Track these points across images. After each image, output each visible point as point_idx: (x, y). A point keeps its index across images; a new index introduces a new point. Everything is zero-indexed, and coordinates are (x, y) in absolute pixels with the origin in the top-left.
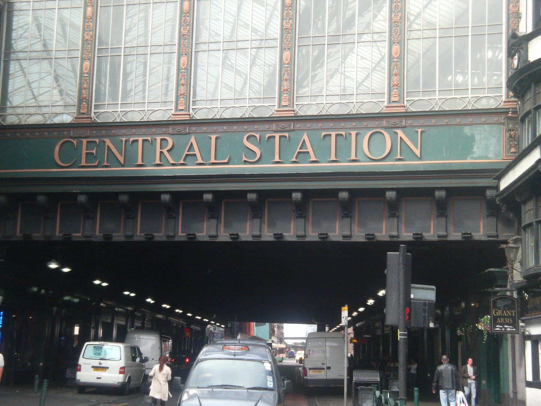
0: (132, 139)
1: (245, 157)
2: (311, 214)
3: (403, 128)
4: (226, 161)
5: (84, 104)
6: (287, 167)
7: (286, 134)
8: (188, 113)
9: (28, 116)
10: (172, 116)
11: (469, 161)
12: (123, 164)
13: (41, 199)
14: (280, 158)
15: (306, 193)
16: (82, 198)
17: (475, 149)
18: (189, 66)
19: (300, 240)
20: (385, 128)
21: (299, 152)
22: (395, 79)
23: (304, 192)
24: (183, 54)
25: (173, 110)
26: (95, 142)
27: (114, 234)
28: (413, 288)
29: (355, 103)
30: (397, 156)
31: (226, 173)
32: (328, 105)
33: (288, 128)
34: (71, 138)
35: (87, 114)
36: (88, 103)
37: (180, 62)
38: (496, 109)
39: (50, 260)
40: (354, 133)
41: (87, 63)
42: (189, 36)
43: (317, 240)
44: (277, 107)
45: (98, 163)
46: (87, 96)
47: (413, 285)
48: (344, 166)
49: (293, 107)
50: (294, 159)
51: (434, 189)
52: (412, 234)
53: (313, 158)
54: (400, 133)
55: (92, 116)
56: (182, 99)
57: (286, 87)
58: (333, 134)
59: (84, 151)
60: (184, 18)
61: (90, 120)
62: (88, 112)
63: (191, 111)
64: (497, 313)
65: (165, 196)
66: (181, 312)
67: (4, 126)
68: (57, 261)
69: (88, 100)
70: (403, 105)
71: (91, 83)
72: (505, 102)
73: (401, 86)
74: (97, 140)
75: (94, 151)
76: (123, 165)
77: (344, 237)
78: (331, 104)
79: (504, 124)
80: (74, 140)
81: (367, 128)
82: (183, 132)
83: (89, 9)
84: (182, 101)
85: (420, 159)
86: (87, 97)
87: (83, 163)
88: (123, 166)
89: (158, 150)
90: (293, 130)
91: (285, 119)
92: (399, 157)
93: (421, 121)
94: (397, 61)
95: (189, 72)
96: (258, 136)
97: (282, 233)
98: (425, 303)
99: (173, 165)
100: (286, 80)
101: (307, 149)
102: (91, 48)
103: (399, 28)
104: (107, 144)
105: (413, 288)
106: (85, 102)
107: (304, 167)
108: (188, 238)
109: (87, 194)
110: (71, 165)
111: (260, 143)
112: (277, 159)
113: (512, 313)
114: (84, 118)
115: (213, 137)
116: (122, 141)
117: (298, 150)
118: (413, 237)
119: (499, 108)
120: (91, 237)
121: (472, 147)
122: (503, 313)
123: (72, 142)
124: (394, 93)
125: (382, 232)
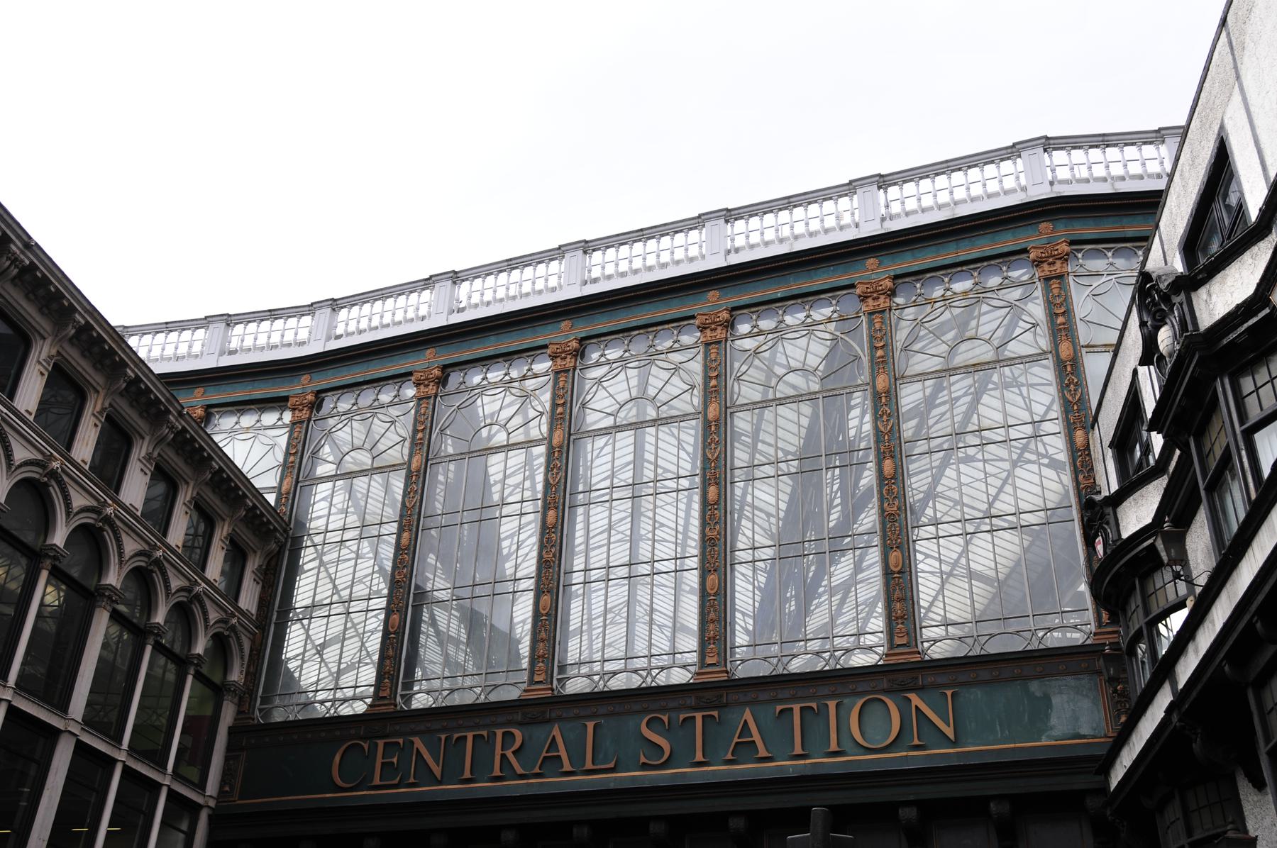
0: (456, 736)
4: (612, 765)
6: (719, 771)
7: (715, 713)
8: (550, 686)
9: (791, 657)
10: (696, 677)
11: (1045, 742)
12: (439, 779)
14: (704, 756)
15: (923, 806)
17: (1054, 721)
18: (554, 609)
20: (886, 692)
21: (545, 757)
22: (711, 628)
23: (749, 815)
30: (409, 778)
34: (361, 738)
35: (390, 699)
36: (392, 681)
37: (705, 585)
42: (405, 582)
45: (400, 779)
48: (821, 762)
50: (729, 757)
54: (915, 699)
55: (554, 687)
56: (541, 664)
59: (379, 761)
60: (709, 513)
62: (390, 696)
63: (555, 682)
65: (907, 810)
69: (393, 675)
70: (916, 649)
72: (1095, 634)
73: (720, 639)
74: (401, 741)
75: (395, 760)
76: (954, 743)
79: (1101, 672)
82: (911, 684)
83: (551, 513)
84: (901, 629)
85: (954, 743)
87: (377, 781)
88: (440, 783)
89: (498, 751)
92: (916, 742)
94: (899, 577)
95: (553, 620)
96: (665, 719)
99: (522, 777)
100: (712, 621)
102: (404, 593)
103: (897, 525)
104: (415, 746)
106: (388, 678)
107: (747, 769)
111: (667, 731)
112: (699, 757)
115: (590, 725)
116: (440, 739)
119: (1087, 645)
121: (1048, 717)
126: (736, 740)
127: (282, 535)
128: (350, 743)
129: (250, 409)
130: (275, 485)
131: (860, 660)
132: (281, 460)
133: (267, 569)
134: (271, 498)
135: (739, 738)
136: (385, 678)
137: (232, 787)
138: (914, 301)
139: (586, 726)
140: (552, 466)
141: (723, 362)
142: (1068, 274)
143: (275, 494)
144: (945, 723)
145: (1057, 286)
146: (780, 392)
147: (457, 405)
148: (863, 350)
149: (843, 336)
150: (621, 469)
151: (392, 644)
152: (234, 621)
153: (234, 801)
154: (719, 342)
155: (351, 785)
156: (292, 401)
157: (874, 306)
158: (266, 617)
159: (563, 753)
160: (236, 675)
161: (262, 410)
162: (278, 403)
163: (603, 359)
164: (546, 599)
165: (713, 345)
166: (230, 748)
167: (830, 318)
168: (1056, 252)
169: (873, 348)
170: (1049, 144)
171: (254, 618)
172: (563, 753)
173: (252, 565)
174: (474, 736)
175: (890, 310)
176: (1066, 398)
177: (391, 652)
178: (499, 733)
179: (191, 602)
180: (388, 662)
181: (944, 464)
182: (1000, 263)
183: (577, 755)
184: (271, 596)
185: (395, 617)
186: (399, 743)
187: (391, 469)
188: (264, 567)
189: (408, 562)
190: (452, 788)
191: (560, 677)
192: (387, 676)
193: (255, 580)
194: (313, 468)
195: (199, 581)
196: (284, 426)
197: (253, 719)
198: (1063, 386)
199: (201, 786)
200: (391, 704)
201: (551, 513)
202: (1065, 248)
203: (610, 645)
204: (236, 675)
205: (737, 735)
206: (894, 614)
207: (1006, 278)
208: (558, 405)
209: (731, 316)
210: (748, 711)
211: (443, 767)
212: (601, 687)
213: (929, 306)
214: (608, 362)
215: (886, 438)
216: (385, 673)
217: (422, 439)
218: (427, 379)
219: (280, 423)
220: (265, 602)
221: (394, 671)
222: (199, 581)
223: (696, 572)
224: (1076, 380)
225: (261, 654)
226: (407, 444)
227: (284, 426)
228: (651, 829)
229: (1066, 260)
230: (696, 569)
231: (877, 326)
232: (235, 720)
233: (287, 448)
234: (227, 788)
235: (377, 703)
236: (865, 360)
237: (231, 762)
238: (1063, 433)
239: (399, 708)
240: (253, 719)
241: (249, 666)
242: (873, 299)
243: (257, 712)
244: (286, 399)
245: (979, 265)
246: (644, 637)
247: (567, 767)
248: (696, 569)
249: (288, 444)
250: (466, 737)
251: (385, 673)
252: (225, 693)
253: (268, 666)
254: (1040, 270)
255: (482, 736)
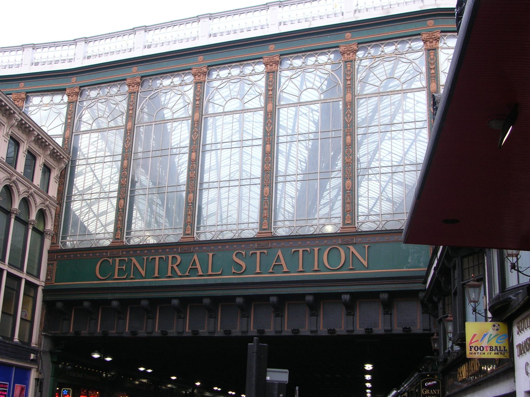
0: (151, 257)
1: (234, 269)
2: (321, 313)
3: (353, 244)
4: (220, 273)
5: (188, 227)
6: (266, 276)
7: (265, 251)
13: (115, 303)
14: (260, 270)
16: (115, 303)
19: (244, 335)
20: (340, 245)
21: (191, 268)
24: (347, 179)
25: (341, 224)
26: (307, 250)
27: (139, 331)
28: (269, 371)
29: (318, 225)
30: (350, 266)
31: (219, 282)
32: (298, 228)
33: (351, 242)
34: (109, 257)
36: (191, 226)
38: (375, 231)
39: (94, 351)
40: (316, 249)
41: (191, 195)
43: (291, 335)
44: (342, 225)
45: (126, 277)
46: (191, 220)
47: (268, 369)
48: (309, 275)
49: (355, 224)
50: (271, 271)
51: (341, 294)
52: (364, 329)
53: (285, 269)
55: (195, 236)
57: (348, 209)
58: (301, 250)
60: (266, 158)
61: (193, 239)
62: (191, 233)
64: (426, 392)
65: (345, 296)
66: (234, 393)
67: (63, 249)
68: (99, 352)
70: (354, 226)
71: (271, 205)
74: (126, 259)
75: (124, 267)
77: (312, 332)
78: (323, 226)
80: (110, 259)
81: (327, 245)
84: (348, 216)
85: (367, 268)
86: (267, 216)
87: (116, 276)
88: (144, 278)
90: (271, 248)
91: (351, 234)
92: (351, 267)
93: (368, 239)
94: (350, 193)
96: (244, 253)
97: (264, 330)
98: (281, 385)
99: (180, 276)
101: (196, 266)
105: (269, 371)
107: (279, 276)
108: (162, 334)
109: (119, 300)
110: (105, 279)
113: (437, 392)
114: (118, 242)
115: (211, 255)
116: (144, 259)
117: (274, 263)
118: (365, 332)
119: (213, 240)
120: (122, 333)
122: (430, 392)
123: (108, 260)
124: (347, 217)
125: (341, 327)
126: (190, 267)
127: (67, 160)
128: (331, 247)
129: (47, 94)
130: (62, 134)
131: (329, 229)
132: (64, 121)
133: (61, 176)
134: (59, 141)
135: (191, 266)
136: (118, 230)
137: (51, 277)
138: (367, 57)
139: (209, 255)
140: (347, 113)
141: (74, 111)
142: (438, 48)
143: (62, 138)
144: (364, 259)
145: (433, 54)
146: (110, 125)
147: (148, 97)
148: (341, 81)
149: (332, 72)
150: (185, 139)
151: (190, 208)
152: (47, 203)
153: (53, 283)
154: (202, 82)
155: (105, 278)
156: (68, 91)
157: (430, 46)
158: (61, 199)
159: (198, 266)
160: (50, 226)
161: (53, 95)
162: (61, 91)
163: (218, 77)
164: (267, 189)
165: (349, 63)
166: (49, 259)
167: (326, 62)
168: (434, 37)
169: (346, 80)
170: (212, 17)
171: (56, 199)
172: (198, 266)
173: (55, 174)
174: (159, 258)
175: (355, 61)
176: (266, 129)
177: (120, 218)
178: (170, 257)
179: (29, 197)
180: (119, 222)
181: (382, 140)
182: (408, 40)
183: (205, 269)
184: (63, 189)
185: (122, 201)
186: (125, 260)
187: (117, 128)
188: (59, 175)
189: (196, 168)
190: (149, 281)
191: (197, 232)
192: (119, 229)
193: (55, 182)
194: (79, 127)
195: (32, 187)
196: (64, 103)
197: (59, 247)
198: (266, 124)
199: (38, 277)
200: (121, 242)
201: (126, 162)
202: (355, 47)
203: (230, 216)
204: (50, 226)
205: (275, 261)
206: (346, 209)
207: (410, 48)
208: (197, 100)
209: (280, 59)
210: (280, 251)
211: (368, 260)
212: (318, 231)
213: (374, 59)
214: (220, 79)
215: (349, 125)
216: (118, 228)
217: (131, 114)
218: (133, 83)
219: (62, 102)
220: (60, 192)
221: (122, 226)
222: (32, 187)
223: (259, 186)
224: (351, 112)
225: (60, 217)
226: (190, 107)
227: (64, 103)
228: (172, 302)
229: (438, 41)
230: (260, 184)
231: (349, 68)
232: (51, 247)
233: (67, 115)
234: (49, 277)
235: (115, 241)
236: (341, 85)
237: (50, 266)
238: (428, 128)
239: (124, 243)
240: (59, 247)
241: (55, 222)
242: (430, 42)
243: (60, 243)
244: (64, 90)
245: (111, 84)
246: (247, 213)
247: (200, 273)
248: (260, 184)
249: (67, 113)
250: (155, 258)
251: (118, 228)
252: (45, 235)
253: (64, 220)
254: (343, 57)
255: (163, 258)
